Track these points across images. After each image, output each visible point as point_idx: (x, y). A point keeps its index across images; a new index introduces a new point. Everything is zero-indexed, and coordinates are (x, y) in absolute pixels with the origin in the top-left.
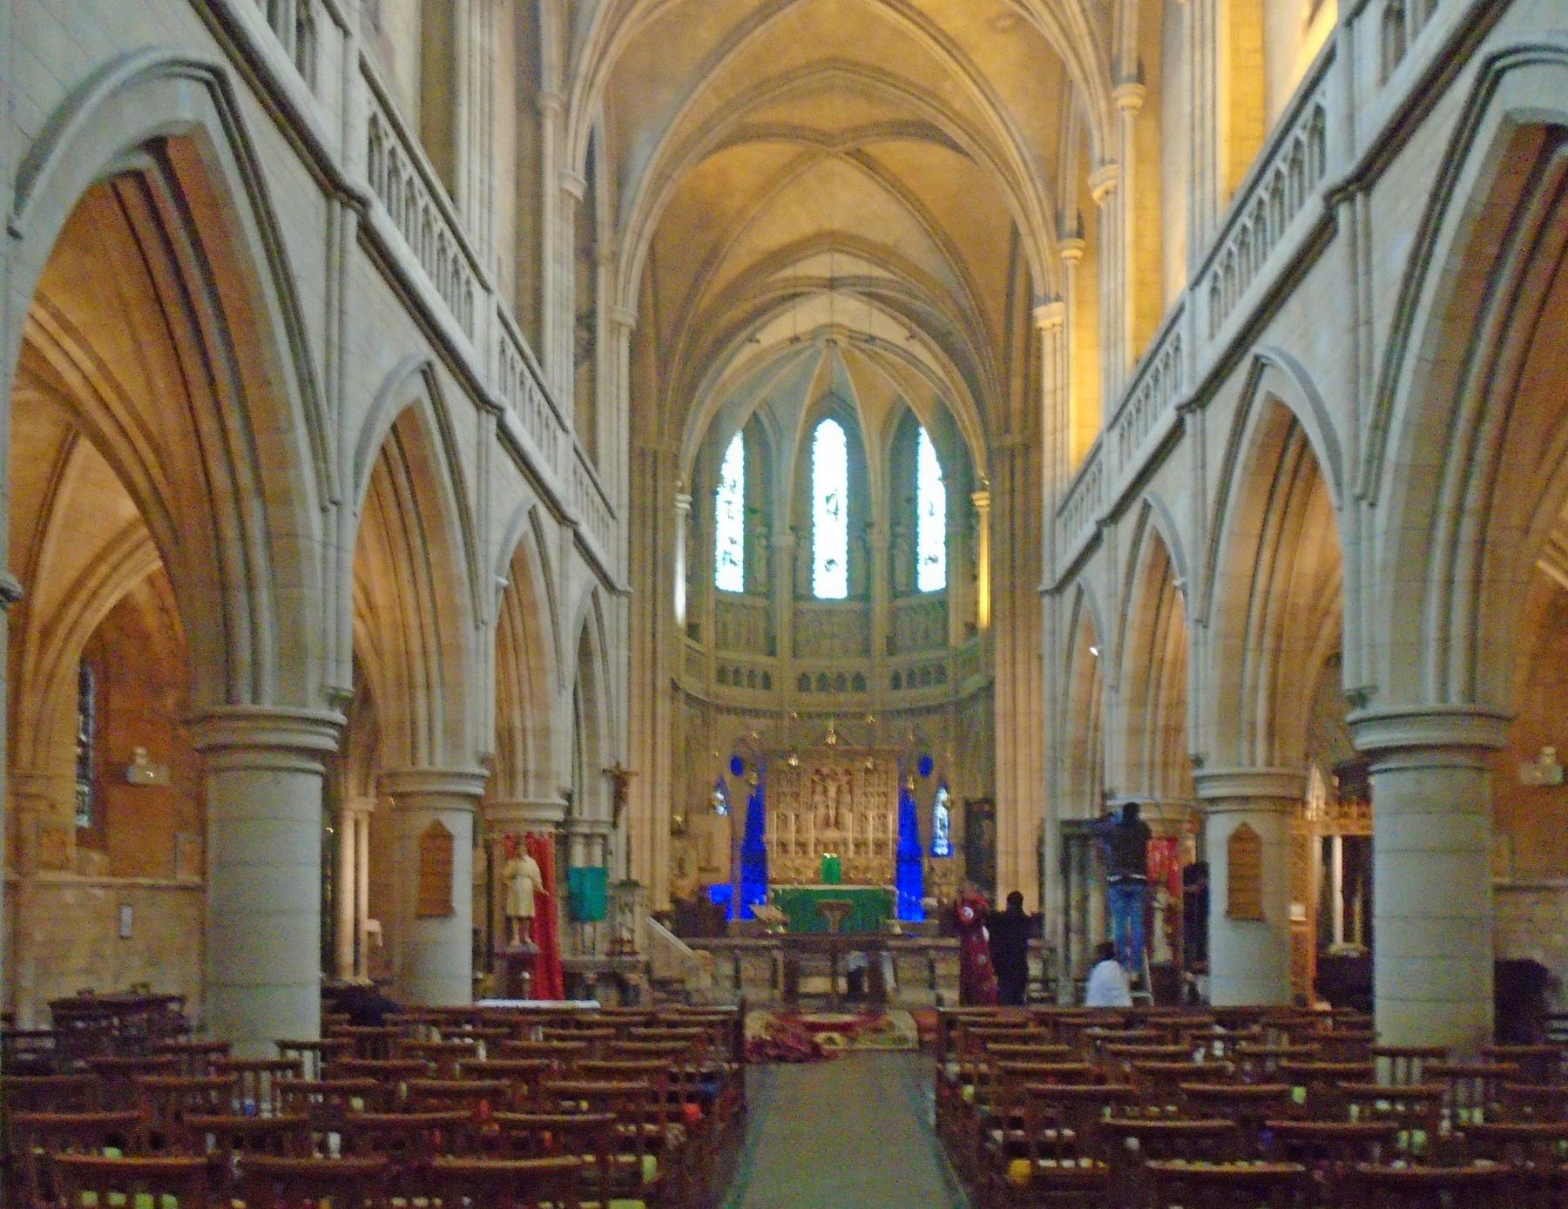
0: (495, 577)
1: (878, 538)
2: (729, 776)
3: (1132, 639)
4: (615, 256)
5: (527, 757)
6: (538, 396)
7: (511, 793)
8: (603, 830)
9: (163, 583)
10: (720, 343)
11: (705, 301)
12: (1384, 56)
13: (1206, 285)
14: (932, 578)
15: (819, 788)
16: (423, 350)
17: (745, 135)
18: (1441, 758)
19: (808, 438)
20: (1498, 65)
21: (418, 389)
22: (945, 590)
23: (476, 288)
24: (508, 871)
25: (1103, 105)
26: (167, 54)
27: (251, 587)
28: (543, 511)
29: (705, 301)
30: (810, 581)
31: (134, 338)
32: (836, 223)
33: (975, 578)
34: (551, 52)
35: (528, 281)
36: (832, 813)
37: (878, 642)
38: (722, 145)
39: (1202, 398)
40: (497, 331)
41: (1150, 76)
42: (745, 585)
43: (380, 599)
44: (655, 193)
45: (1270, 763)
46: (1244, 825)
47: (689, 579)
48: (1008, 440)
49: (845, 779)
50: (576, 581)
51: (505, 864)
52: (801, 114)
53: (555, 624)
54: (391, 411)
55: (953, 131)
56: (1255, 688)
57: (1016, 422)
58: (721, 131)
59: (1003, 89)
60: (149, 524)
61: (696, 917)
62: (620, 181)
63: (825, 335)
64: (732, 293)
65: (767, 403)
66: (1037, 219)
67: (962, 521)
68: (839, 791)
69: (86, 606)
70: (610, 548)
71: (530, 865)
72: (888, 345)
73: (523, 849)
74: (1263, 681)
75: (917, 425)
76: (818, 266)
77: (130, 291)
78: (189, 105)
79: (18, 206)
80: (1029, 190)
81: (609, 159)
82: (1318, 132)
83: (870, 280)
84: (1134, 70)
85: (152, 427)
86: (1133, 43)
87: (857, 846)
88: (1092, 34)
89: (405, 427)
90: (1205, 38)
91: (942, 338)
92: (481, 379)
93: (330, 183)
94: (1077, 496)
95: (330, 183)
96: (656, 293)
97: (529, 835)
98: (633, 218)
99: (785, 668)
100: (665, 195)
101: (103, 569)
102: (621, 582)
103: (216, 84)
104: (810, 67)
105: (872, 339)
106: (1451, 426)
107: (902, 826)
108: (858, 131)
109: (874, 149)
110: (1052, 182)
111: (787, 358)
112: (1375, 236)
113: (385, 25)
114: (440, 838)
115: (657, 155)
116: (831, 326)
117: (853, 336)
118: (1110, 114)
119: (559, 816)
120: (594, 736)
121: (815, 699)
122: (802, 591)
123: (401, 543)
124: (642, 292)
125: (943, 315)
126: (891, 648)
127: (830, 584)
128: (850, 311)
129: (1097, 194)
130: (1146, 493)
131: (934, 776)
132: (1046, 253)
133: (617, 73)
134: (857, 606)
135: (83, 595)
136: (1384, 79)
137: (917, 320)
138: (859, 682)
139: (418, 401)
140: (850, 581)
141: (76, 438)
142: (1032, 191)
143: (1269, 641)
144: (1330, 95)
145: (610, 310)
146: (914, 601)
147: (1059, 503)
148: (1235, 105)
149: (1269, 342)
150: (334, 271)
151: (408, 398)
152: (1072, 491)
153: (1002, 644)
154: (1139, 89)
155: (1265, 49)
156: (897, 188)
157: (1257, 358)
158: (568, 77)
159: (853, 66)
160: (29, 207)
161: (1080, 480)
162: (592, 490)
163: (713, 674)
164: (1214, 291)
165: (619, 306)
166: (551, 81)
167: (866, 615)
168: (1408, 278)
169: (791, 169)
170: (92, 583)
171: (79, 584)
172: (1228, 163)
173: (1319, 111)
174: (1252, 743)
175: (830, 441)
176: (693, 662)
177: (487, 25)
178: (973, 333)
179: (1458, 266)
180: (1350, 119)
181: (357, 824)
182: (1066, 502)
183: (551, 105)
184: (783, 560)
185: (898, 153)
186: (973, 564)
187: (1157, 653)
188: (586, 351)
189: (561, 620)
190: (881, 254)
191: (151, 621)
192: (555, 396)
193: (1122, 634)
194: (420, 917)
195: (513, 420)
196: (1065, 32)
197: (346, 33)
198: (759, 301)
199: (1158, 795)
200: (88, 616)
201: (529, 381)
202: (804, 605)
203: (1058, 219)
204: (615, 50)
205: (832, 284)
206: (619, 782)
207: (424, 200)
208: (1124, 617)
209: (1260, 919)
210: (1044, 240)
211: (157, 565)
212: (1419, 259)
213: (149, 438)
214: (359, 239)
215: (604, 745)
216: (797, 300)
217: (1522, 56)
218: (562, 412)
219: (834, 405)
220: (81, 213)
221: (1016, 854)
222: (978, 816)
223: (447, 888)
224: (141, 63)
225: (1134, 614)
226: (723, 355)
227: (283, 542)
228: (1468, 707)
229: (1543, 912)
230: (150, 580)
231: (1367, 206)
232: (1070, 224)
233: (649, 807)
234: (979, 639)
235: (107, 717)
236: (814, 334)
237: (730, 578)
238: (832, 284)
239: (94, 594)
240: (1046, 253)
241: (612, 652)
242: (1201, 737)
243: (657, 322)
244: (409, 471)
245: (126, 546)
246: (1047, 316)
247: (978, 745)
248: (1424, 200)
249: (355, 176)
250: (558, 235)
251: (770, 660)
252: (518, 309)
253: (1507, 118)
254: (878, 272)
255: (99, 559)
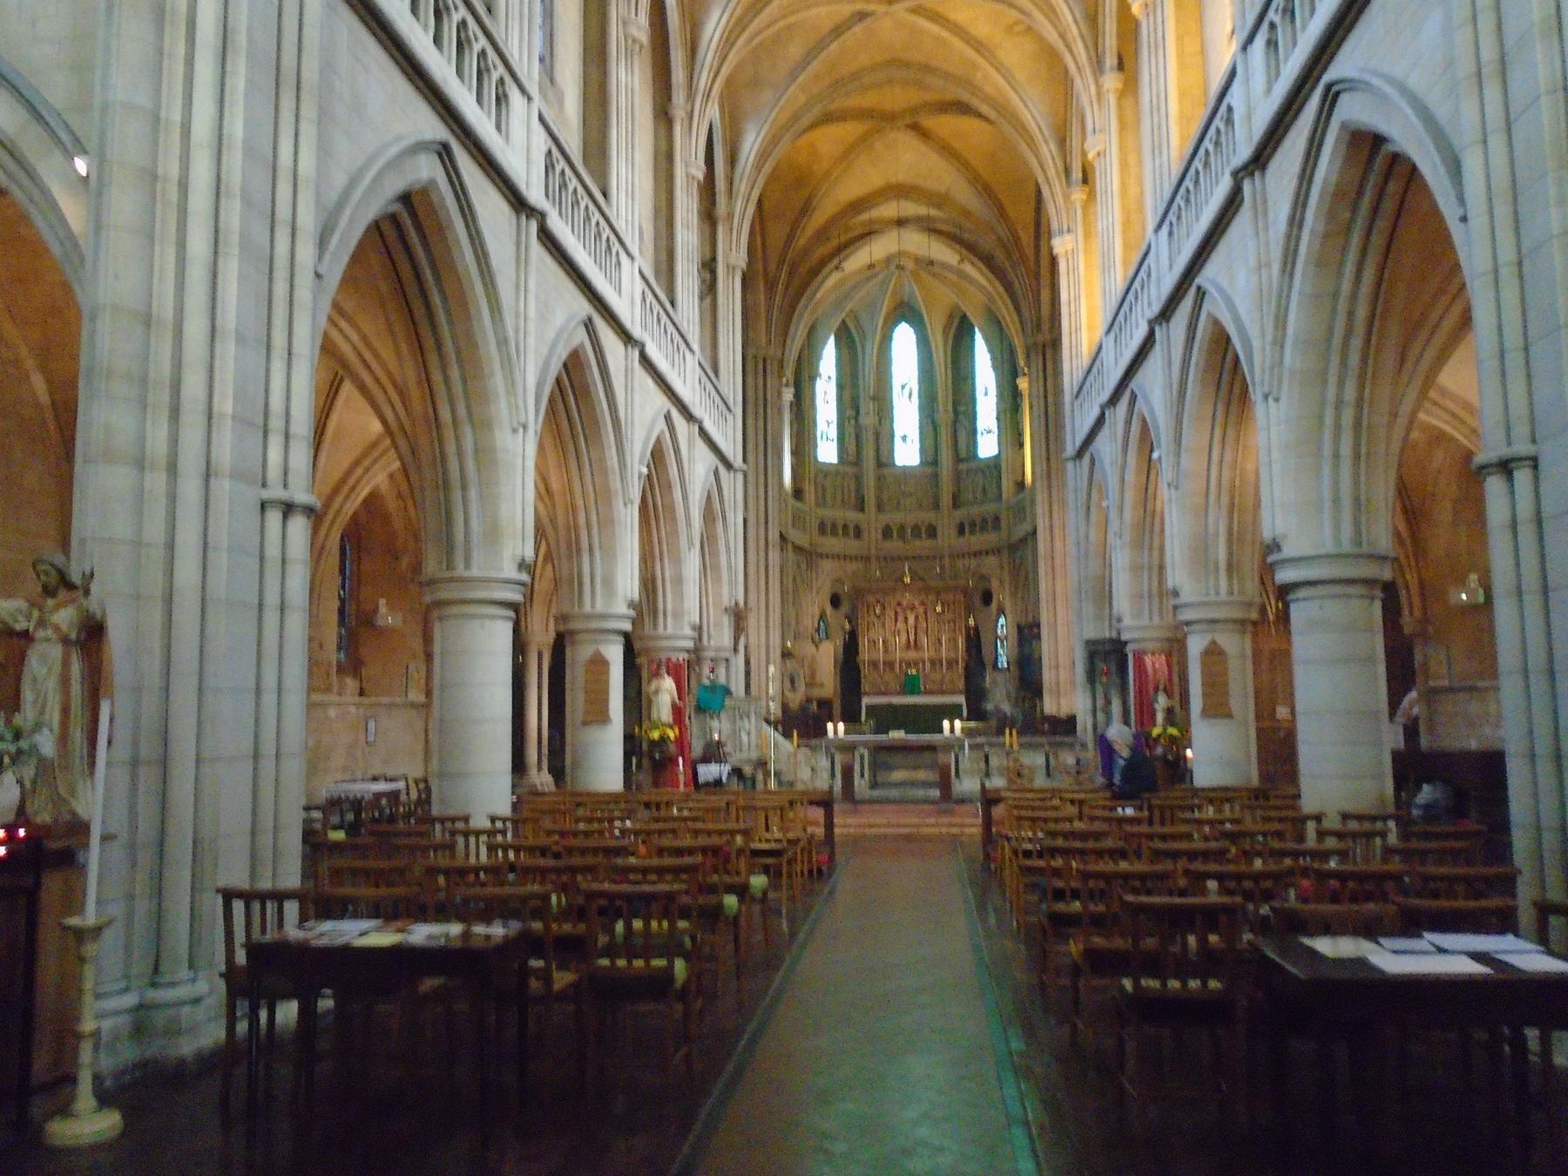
0: (638, 467)
1: (944, 416)
2: (829, 609)
3: (1130, 496)
4: (730, 216)
5: (666, 599)
6: (671, 328)
7: (655, 626)
8: (727, 654)
9: (400, 478)
10: (815, 272)
11: (801, 241)
12: (1268, 73)
13: (1165, 229)
14: (987, 446)
15: (901, 618)
16: (584, 308)
17: (828, 118)
18: (1337, 589)
19: (886, 339)
20: (1335, 89)
21: (581, 336)
22: (997, 457)
23: (623, 257)
24: (653, 686)
25: (1093, 89)
26: (412, 140)
27: (464, 488)
28: (675, 414)
29: (801, 241)
30: (892, 451)
31: (387, 319)
32: (902, 178)
33: (1021, 445)
34: (678, 75)
35: (663, 243)
36: (912, 638)
37: (946, 499)
38: (813, 126)
39: (1166, 314)
40: (639, 285)
41: (1126, 64)
42: (840, 457)
43: (555, 485)
44: (758, 167)
45: (1231, 593)
46: (1214, 643)
47: (793, 453)
48: (1040, 338)
49: (921, 610)
50: (700, 465)
51: (649, 682)
52: (869, 100)
53: (685, 497)
54: (562, 353)
55: (984, 109)
56: (1217, 534)
57: (1046, 326)
58: (805, 121)
59: (1020, 76)
60: (396, 448)
61: (802, 722)
62: (732, 160)
63: (893, 261)
64: (822, 234)
65: (854, 315)
66: (1052, 172)
67: (1010, 402)
68: (917, 618)
69: (347, 497)
70: (729, 438)
71: (668, 683)
72: (944, 266)
73: (663, 670)
74: (1222, 530)
75: (972, 327)
76: (889, 210)
77: (385, 287)
78: (427, 169)
79: (320, 258)
80: (1044, 150)
81: (720, 152)
82: (1229, 121)
83: (928, 218)
84: (1115, 62)
85: (398, 378)
86: (1114, 43)
87: (933, 662)
88: (1082, 37)
89: (573, 365)
90: (1159, 46)
91: (987, 260)
92: (627, 323)
93: (519, 203)
94: (1088, 384)
95: (519, 203)
96: (763, 237)
97: (669, 660)
98: (742, 187)
99: (872, 521)
100: (768, 168)
101: (359, 471)
102: (738, 461)
103: (444, 152)
104: (875, 67)
105: (932, 263)
106: (1329, 340)
107: (968, 650)
108: (914, 110)
109: (928, 122)
110: (1062, 142)
111: (868, 279)
112: (1270, 203)
113: (559, 78)
114: (600, 663)
115: (760, 139)
116: (900, 254)
117: (917, 260)
118: (1099, 94)
119: (690, 644)
120: (718, 580)
121: (894, 546)
122: (884, 460)
123: (571, 447)
124: (752, 233)
125: (987, 243)
126: (956, 503)
127: (907, 453)
128: (916, 242)
129: (1090, 156)
130: (1133, 385)
131: (994, 605)
132: (1060, 199)
133: (729, 82)
134: (929, 470)
135: (346, 490)
136: (1269, 90)
137: (969, 247)
138: (932, 532)
139: (582, 345)
140: (922, 451)
141: (342, 380)
142: (1049, 150)
143: (1225, 500)
144: (1235, 97)
145: (726, 256)
146: (973, 465)
147: (1076, 390)
148: (1182, 95)
149: (1210, 274)
150: (521, 260)
151: (575, 343)
152: (1085, 379)
153: (1041, 498)
154: (1120, 76)
155: (1203, 51)
156: (947, 151)
157: (1199, 288)
158: (691, 96)
159: (906, 65)
160: (327, 257)
161: (1089, 371)
162: (713, 392)
163: (815, 531)
164: (1170, 234)
165: (734, 254)
166: (679, 97)
167: (936, 476)
168: (1288, 236)
169: (863, 140)
170: (351, 482)
171: (343, 480)
172: (1177, 143)
173: (1230, 109)
174: (1217, 579)
175: (904, 340)
176: (798, 520)
177: (630, 69)
178: (1009, 256)
179: (1321, 228)
180: (1249, 118)
181: (540, 655)
182: (1081, 388)
183: (679, 113)
184: (869, 437)
185: (945, 125)
186: (1020, 435)
187: (1149, 507)
188: (709, 288)
189: (691, 498)
190: (939, 200)
191: (392, 505)
192: (684, 327)
193: (1122, 492)
194: (585, 723)
195: (653, 351)
196: (1062, 36)
197: (530, 99)
198: (843, 239)
199: (1156, 618)
200: (348, 505)
201: (664, 318)
202: (886, 471)
203: (1067, 171)
204: (725, 71)
205: (900, 223)
206: (739, 618)
207: (585, 201)
208: (1123, 480)
209: (1230, 716)
210: (1058, 189)
211: (397, 464)
212: (1296, 221)
213: (395, 385)
214: (539, 237)
215: (725, 590)
216: (873, 237)
217: (1350, 85)
218: (690, 338)
219: (905, 311)
220: (357, 258)
221: (1057, 667)
222: (1028, 633)
223: (605, 702)
224: (395, 150)
225: (1130, 477)
226: (815, 284)
227: (486, 455)
228: (1356, 550)
229: (1474, 708)
230: (391, 476)
231: (1263, 183)
232: (1077, 174)
233: (764, 634)
234: (1026, 493)
235: (359, 582)
236: (888, 260)
237: (827, 452)
238: (900, 223)
239: (353, 488)
240: (1060, 199)
241: (730, 516)
242: (1178, 575)
243: (765, 259)
244: (574, 398)
245: (376, 454)
246: (1061, 245)
247: (1024, 578)
248: (1295, 182)
249: (535, 195)
250: (687, 207)
251: (860, 516)
252: (657, 273)
253: (1344, 126)
254: (933, 212)
255: (356, 464)
